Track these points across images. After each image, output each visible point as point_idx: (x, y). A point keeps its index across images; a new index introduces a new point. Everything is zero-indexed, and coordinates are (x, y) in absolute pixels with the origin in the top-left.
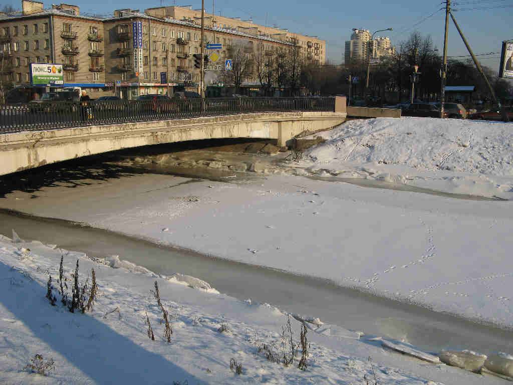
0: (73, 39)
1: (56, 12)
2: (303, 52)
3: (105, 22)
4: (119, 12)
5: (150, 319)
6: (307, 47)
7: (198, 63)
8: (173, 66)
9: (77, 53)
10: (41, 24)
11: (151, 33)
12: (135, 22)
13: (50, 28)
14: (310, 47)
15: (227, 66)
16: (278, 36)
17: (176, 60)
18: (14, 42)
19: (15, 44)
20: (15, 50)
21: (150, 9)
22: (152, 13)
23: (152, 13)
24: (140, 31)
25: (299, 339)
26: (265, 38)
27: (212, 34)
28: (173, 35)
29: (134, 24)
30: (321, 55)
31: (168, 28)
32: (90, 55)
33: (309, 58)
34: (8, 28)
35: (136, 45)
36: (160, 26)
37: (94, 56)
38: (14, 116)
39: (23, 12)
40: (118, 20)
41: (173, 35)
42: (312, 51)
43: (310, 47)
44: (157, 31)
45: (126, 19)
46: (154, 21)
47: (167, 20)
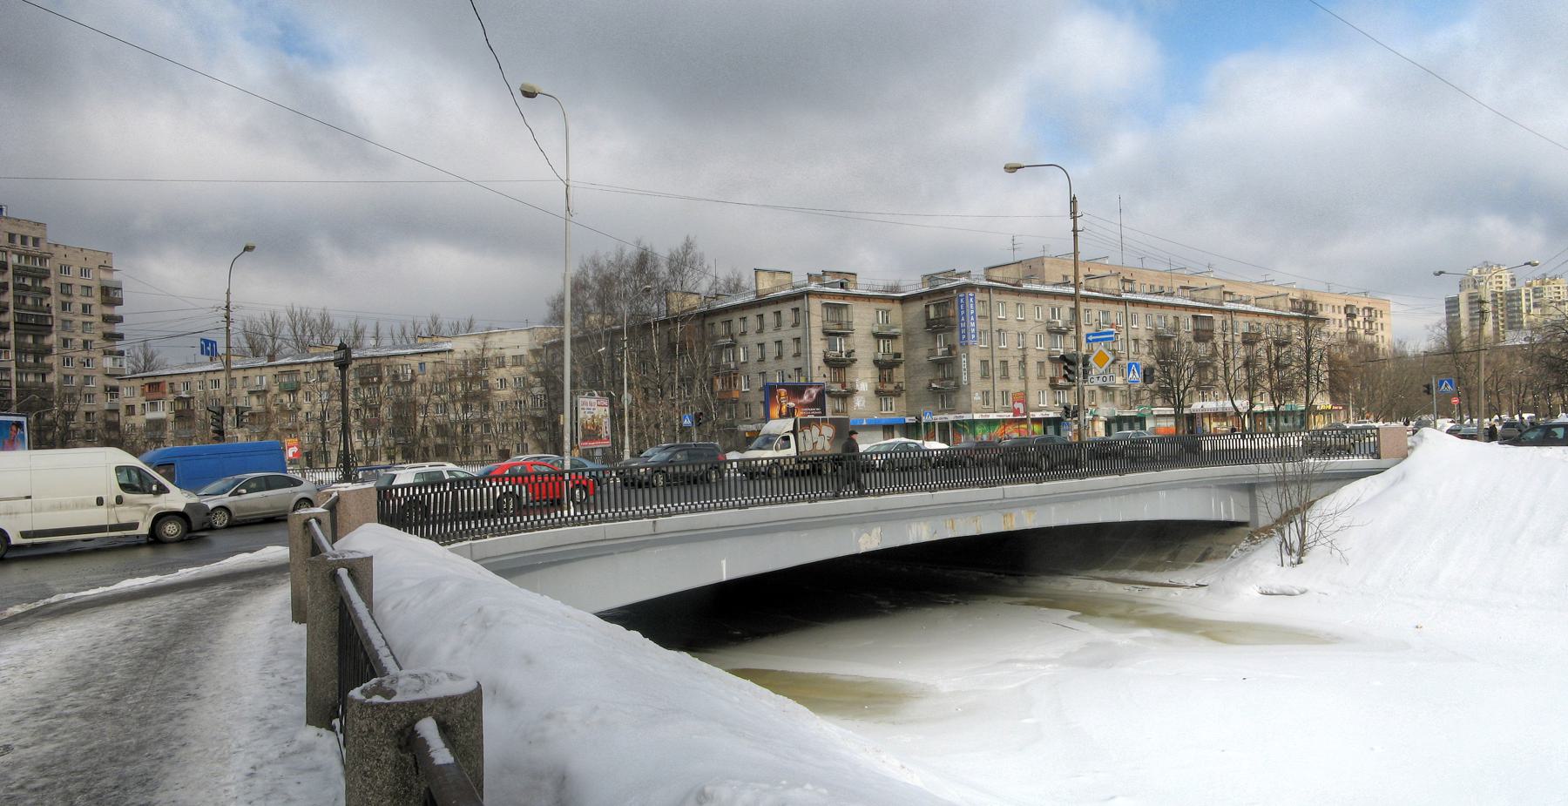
0: (186, 417)
1: (813, 286)
2: (1336, 326)
3: (903, 300)
4: (931, 278)
5: (183, 728)
6: (1343, 317)
7: (1070, 372)
8: (1041, 377)
9: (854, 361)
10: (786, 311)
11: (994, 314)
12: (961, 295)
13: (800, 318)
14: (1351, 316)
15: (1131, 375)
16: (1270, 302)
17: (1048, 365)
18: (741, 346)
19: (741, 350)
20: (742, 360)
21: (990, 268)
22: (997, 274)
23: (997, 274)
24: (972, 312)
25: (298, 672)
26: (1241, 307)
27: (1121, 308)
28: (1038, 317)
29: (960, 298)
30: (1380, 333)
31: (1029, 302)
32: (876, 362)
33: (1352, 342)
34: (762, 315)
35: (966, 339)
36: (1011, 300)
37: (884, 367)
38: (473, 513)
39: (757, 291)
40: (928, 294)
41: (1038, 317)
42: (1359, 326)
43: (1351, 316)
44: (1007, 311)
45: (943, 291)
46: (1000, 290)
47: (1026, 286)
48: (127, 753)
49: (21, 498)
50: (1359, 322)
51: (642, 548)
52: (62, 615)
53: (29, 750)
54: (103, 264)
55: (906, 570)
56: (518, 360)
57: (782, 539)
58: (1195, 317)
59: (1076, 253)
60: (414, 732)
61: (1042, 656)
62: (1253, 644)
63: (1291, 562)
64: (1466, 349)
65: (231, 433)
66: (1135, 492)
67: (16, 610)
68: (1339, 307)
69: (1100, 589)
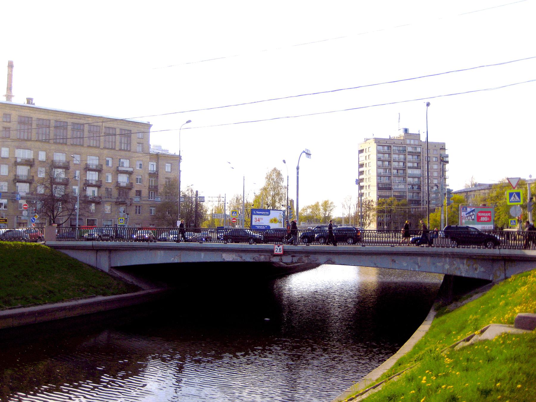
48: (334, 333)
49: (281, 118)
50: (147, 235)
51: (513, 257)
52: (521, 257)
53: (380, 388)
54: (442, 147)
55: (506, 352)
56: (9, 369)
57: (161, 253)
58: (89, 125)
59: (427, 141)
60: (40, 161)
61: (6, 194)
62: (381, 139)
63: (60, 162)
64: (436, 165)
65: (335, 226)
66: (78, 249)
67: (118, 274)
68: (366, 186)
69: (522, 182)
